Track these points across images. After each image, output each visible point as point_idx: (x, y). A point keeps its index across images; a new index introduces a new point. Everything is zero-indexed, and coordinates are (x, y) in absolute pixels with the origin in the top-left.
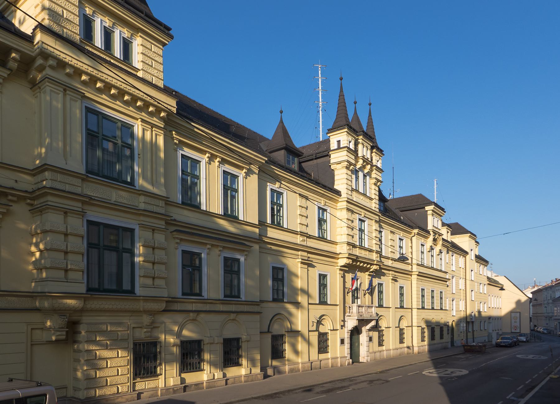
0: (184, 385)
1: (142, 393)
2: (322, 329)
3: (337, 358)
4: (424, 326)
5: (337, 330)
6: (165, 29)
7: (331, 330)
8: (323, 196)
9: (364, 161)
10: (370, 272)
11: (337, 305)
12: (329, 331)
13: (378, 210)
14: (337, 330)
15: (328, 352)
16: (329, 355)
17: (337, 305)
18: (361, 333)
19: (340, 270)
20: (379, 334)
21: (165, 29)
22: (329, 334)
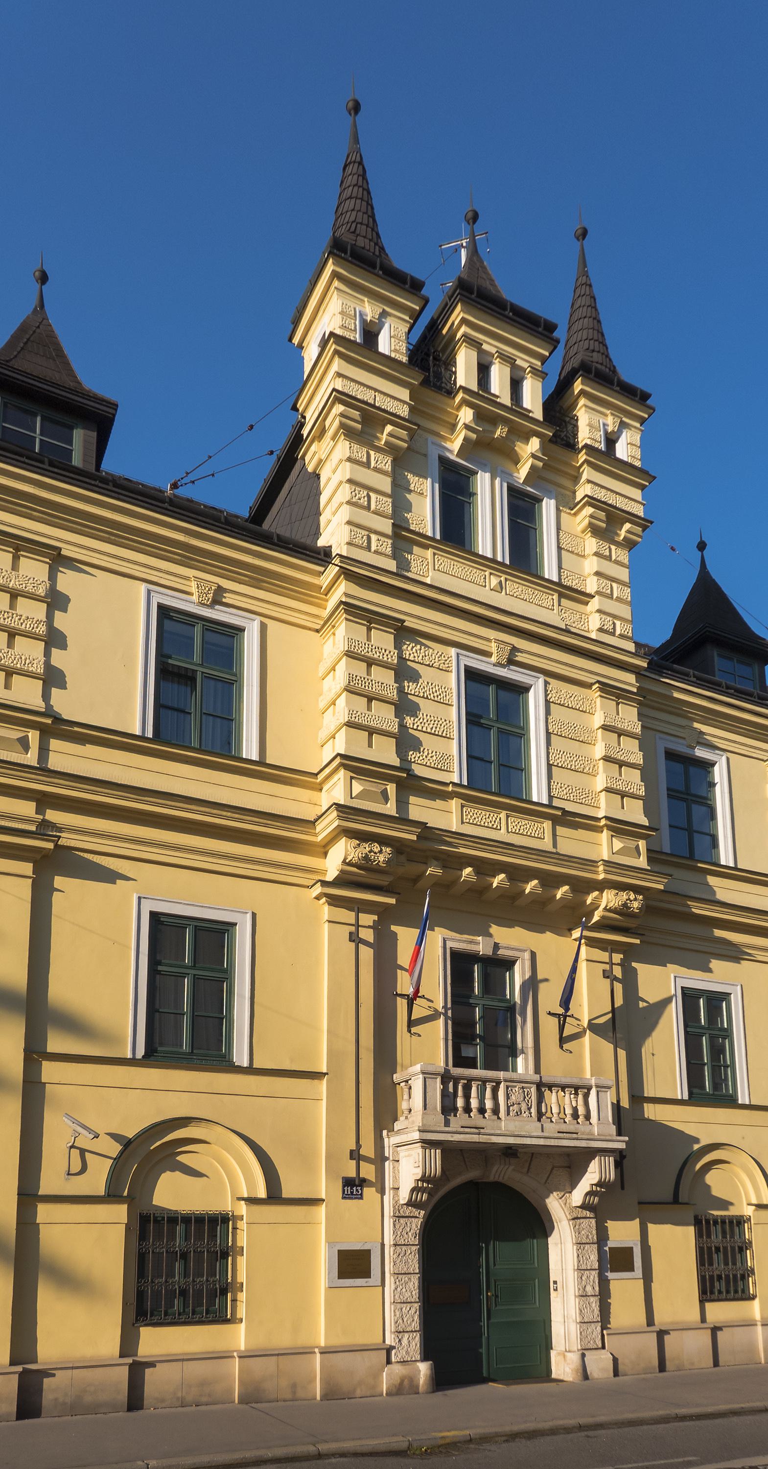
0: (130, 1360)
1: (152, 1365)
2: (171, 1193)
3: (307, 1352)
4: (733, 1212)
5: (315, 1202)
6: (639, 397)
7: (252, 1201)
8: (189, 557)
9: (480, 416)
10: (586, 927)
11: (317, 1076)
12: (242, 1209)
13: (631, 647)
14: (315, 1202)
15: (233, 1320)
16: (238, 1337)
17: (317, 1076)
18: (552, 1228)
19: (335, 901)
20: (699, 1235)
21: (639, 397)
22: (242, 1225)
